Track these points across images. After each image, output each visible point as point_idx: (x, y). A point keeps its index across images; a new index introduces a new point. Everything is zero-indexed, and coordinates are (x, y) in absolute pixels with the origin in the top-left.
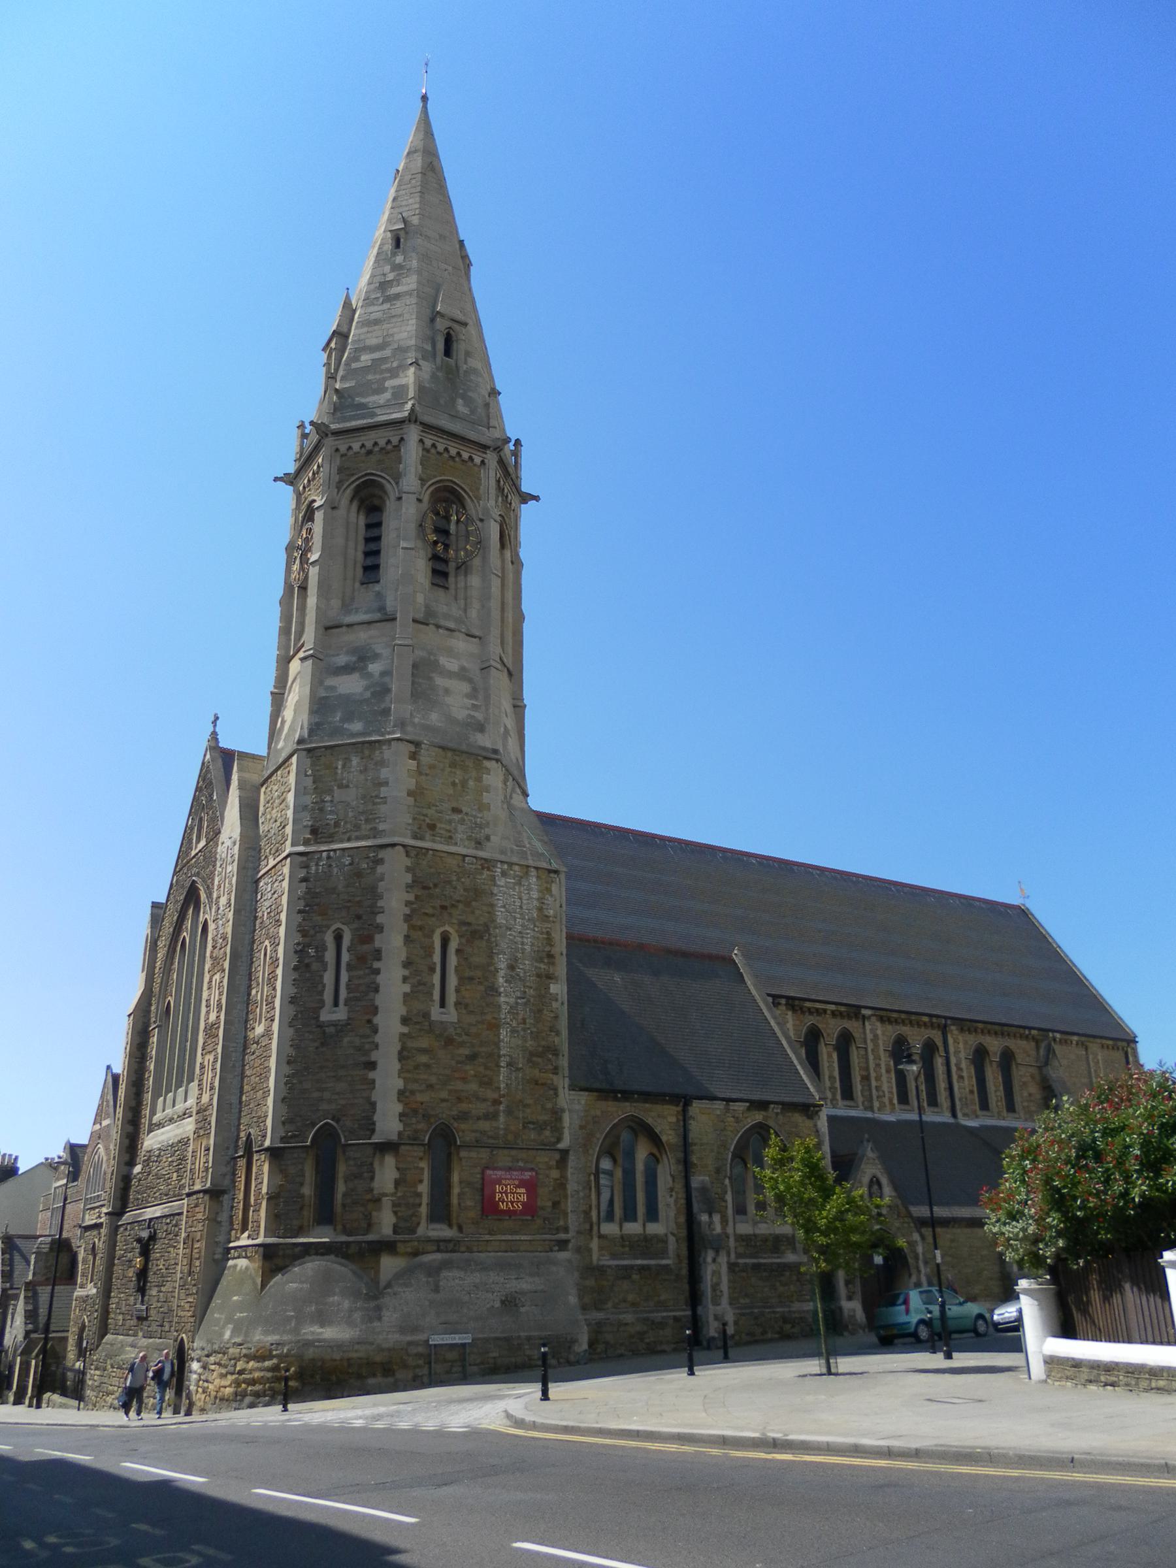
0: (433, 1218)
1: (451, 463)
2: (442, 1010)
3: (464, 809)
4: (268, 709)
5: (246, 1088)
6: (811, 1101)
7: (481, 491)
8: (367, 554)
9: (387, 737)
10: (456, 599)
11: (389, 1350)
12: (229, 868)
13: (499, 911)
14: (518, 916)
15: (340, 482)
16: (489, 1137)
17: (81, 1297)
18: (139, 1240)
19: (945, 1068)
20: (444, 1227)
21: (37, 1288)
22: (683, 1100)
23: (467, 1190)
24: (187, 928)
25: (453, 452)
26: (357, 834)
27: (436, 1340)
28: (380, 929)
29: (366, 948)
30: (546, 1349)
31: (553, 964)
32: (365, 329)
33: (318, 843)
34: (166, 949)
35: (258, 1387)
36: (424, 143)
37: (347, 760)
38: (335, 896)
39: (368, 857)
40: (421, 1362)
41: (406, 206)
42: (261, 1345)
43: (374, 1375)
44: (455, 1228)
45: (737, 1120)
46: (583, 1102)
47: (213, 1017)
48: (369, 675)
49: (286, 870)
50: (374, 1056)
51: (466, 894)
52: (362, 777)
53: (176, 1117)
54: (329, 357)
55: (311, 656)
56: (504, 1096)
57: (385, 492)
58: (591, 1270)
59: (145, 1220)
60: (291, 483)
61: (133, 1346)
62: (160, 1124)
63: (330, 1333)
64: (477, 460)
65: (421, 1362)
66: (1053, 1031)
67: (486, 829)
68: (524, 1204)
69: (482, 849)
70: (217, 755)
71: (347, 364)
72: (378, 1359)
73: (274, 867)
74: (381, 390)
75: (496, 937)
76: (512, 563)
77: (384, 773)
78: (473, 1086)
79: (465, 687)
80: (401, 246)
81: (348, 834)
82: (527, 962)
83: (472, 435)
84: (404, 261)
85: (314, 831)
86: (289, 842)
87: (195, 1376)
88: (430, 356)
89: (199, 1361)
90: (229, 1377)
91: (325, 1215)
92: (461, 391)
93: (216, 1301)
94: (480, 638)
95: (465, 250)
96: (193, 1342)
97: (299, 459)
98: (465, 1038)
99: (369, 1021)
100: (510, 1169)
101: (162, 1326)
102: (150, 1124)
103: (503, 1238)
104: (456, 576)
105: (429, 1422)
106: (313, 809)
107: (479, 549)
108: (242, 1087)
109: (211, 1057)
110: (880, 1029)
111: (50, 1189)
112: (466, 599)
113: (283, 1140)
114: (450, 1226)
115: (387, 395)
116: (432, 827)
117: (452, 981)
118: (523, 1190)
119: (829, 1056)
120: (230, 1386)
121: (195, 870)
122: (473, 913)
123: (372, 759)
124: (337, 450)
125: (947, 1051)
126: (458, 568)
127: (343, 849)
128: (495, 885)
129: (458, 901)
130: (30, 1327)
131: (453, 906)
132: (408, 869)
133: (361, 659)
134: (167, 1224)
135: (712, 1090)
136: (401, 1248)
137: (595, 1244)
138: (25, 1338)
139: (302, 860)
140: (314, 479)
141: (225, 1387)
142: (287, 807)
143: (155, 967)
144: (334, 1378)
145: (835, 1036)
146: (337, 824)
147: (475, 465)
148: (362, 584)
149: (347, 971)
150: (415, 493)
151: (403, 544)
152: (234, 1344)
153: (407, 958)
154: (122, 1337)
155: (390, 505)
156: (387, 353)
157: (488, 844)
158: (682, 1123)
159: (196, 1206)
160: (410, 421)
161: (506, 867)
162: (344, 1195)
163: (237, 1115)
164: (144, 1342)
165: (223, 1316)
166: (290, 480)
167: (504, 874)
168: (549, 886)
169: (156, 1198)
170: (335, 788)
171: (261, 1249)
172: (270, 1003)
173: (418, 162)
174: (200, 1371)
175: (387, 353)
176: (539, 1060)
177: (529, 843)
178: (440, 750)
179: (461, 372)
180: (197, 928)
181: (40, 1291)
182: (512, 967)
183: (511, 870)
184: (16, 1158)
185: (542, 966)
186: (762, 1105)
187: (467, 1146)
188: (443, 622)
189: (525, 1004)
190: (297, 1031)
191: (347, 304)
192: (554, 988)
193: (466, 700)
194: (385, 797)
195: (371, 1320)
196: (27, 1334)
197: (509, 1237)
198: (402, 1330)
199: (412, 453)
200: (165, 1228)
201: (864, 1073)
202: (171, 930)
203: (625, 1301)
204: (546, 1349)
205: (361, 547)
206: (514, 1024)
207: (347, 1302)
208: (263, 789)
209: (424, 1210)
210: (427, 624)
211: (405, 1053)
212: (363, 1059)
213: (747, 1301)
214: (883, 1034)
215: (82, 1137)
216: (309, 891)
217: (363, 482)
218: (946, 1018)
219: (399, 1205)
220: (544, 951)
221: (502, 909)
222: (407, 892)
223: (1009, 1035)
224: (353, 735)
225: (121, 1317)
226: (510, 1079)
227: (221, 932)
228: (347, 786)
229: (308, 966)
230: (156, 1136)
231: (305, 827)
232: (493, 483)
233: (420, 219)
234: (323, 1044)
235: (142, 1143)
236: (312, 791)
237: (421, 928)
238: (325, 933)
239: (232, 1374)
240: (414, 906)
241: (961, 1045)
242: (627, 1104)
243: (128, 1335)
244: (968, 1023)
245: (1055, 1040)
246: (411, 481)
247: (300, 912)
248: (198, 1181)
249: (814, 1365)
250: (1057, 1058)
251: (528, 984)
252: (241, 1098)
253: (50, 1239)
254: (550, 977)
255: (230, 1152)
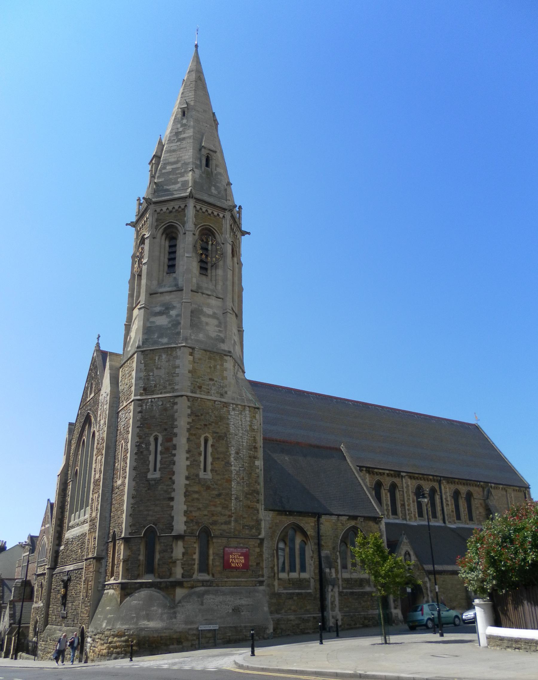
0: (201, 571)
1: (209, 217)
2: (205, 473)
3: (215, 379)
4: (123, 332)
5: (113, 509)
6: (377, 516)
7: (223, 230)
8: (170, 260)
9: (179, 345)
10: (211, 280)
11: (180, 632)
12: (105, 407)
13: (231, 427)
14: (240, 429)
15: (157, 226)
16: (227, 533)
17: (36, 608)
18: (63, 581)
19: (440, 500)
20: (206, 574)
21: (15, 603)
22: (317, 515)
23: (216, 557)
24: (85, 435)
25: (210, 212)
26: (165, 390)
27: (202, 628)
28: (176, 435)
29: (169, 444)
30: (254, 632)
31: (257, 451)
32: (169, 154)
33: (147, 395)
34: (75, 444)
35: (118, 650)
36: (196, 67)
37: (160, 356)
38: (155, 420)
39: (170, 402)
40: (195, 638)
41: (188, 96)
42: (120, 630)
43: (173, 644)
44: (211, 575)
45: (343, 525)
46: (271, 516)
47: (97, 476)
48: (171, 316)
49: (132, 408)
50: (173, 495)
51: (216, 419)
52: (167, 364)
53: (80, 523)
54: (152, 167)
55: (143, 307)
56: (234, 513)
57: (178, 230)
58: (274, 595)
59: (66, 572)
60: (134, 226)
61: (60, 630)
62: (73, 526)
63: (152, 624)
64: (221, 215)
65: (195, 638)
66: (491, 483)
67: (225, 389)
68: (243, 564)
69: (223, 398)
70: (99, 353)
71: (160, 170)
72: (175, 636)
73: (126, 406)
74: (176, 183)
75: (230, 439)
76: (238, 264)
77: (178, 362)
78: (219, 509)
79: (215, 322)
80: (186, 115)
81: (161, 391)
82: (244, 451)
83: (219, 204)
84: (187, 122)
85: (145, 389)
86: (133, 395)
87: (89, 645)
88: (199, 167)
89: (91, 637)
90: (105, 645)
91: (150, 569)
92: (213, 183)
93: (99, 609)
94: (222, 299)
95: (216, 117)
96: (88, 629)
97: (138, 215)
98: (216, 486)
99: (171, 478)
100: (236, 548)
101: (73, 621)
102: (68, 527)
103: (233, 580)
104: (211, 270)
105: (199, 666)
106: (144, 379)
107: (222, 257)
108: (111, 509)
109: (97, 495)
110: (409, 482)
111: (21, 557)
112: (216, 280)
113: (130, 534)
114: (208, 574)
115: (179, 185)
116: (200, 387)
117: (210, 460)
118: (242, 557)
119: (386, 495)
120: (105, 649)
121: (89, 408)
122: (219, 427)
123: (172, 356)
124: (156, 211)
125: (441, 492)
126: (212, 266)
127: (158, 398)
128: (229, 414)
129: (212, 422)
130: (12, 621)
131: (210, 424)
132: (189, 407)
133: (167, 309)
134: (76, 573)
135: (331, 510)
136: (185, 584)
137: (276, 583)
138: (9, 627)
139: (139, 403)
140: (145, 224)
141: (103, 650)
142: (132, 378)
143: (70, 453)
144: (154, 645)
145: (389, 485)
146: (155, 386)
147: (220, 218)
148: (167, 273)
149: (160, 455)
150: (192, 231)
151: (186, 255)
152: (107, 629)
153: (188, 449)
154: (54, 626)
155: (180, 236)
156: (179, 165)
157: (226, 395)
158: (317, 526)
159: (90, 565)
160: (190, 197)
161: (234, 406)
162: (159, 560)
163: (109, 522)
164: (65, 628)
165: (102, 617)
166: (134, 225)
167: (234, 409)
168: (254, 415)
169: (71, 561)
170: (155, 369)
171: (120, 585)
172: (124, 470)
173: (193, 76)
174: (91, 642)
175: (179, 165)
176: (250, 496)
177: (245, 395)
178: (204, 351)
179: (214, 174)
180: (90, 434)
181: (16, 605)
182: (237, 453)
183: (237, 407)
184: (5, 543)
185: (252, 452)
186: (354, 518)
187: (216, 537)
188: (205, 292)
189: (244, 470)
190: (137, 483)
191: (160, 142)
192: (257, 463)
193: (216, 328)
194: (178, 373)
195: (171, 618)
196: (11, 625)
197: (236, 580)
198: (186, 623)
199: (190, 212)
200: (75, 575)
201: (402, 503)
202: (78, 435)
203: (290, 609)
204: (254, 632)
205: (167, 256)
206: (238, 480)
207: (160, 610)
208: (121, 370)
209: (196, 567)
210: (198, 292)
211: (187, 493)
212: (168, 496)
213: (347, 609)
214: (411, 485)
215: (36, 533)
216: (142, 417)
217: (167, 226)
218: (440, 477)
219: (184, 564)
220: (252, 446)
221: (233, 426)
222: (188, 418)
223: (470, 485)
224: (163, 344)
225: (54, 617)
226: (237, 505)
227: (101, 436)
228: (160, 368)
229: (142, 452)
230: (71, 532)
231: (140, 387)
232: (228, 226)
233: (194, 102)
234: (149, 489)
235: (64, 535)
236: (144, 371)
237: (195, 435)
238: (150, 437)
239: (106, 643)
240: (192, 424)
241: (448, 490)
242: (291, 517)
243: (58, 625)
244: (451, 479)
245: (491, 487)
246: (190, 225)
247: (138, 427)
248: (90, 553)
249: (379, 639)
250: (492, 496)
251: (245, 461)
252: (110, 514)
253: (21, 580)
254: (255, 458)
255: (105, 540)
